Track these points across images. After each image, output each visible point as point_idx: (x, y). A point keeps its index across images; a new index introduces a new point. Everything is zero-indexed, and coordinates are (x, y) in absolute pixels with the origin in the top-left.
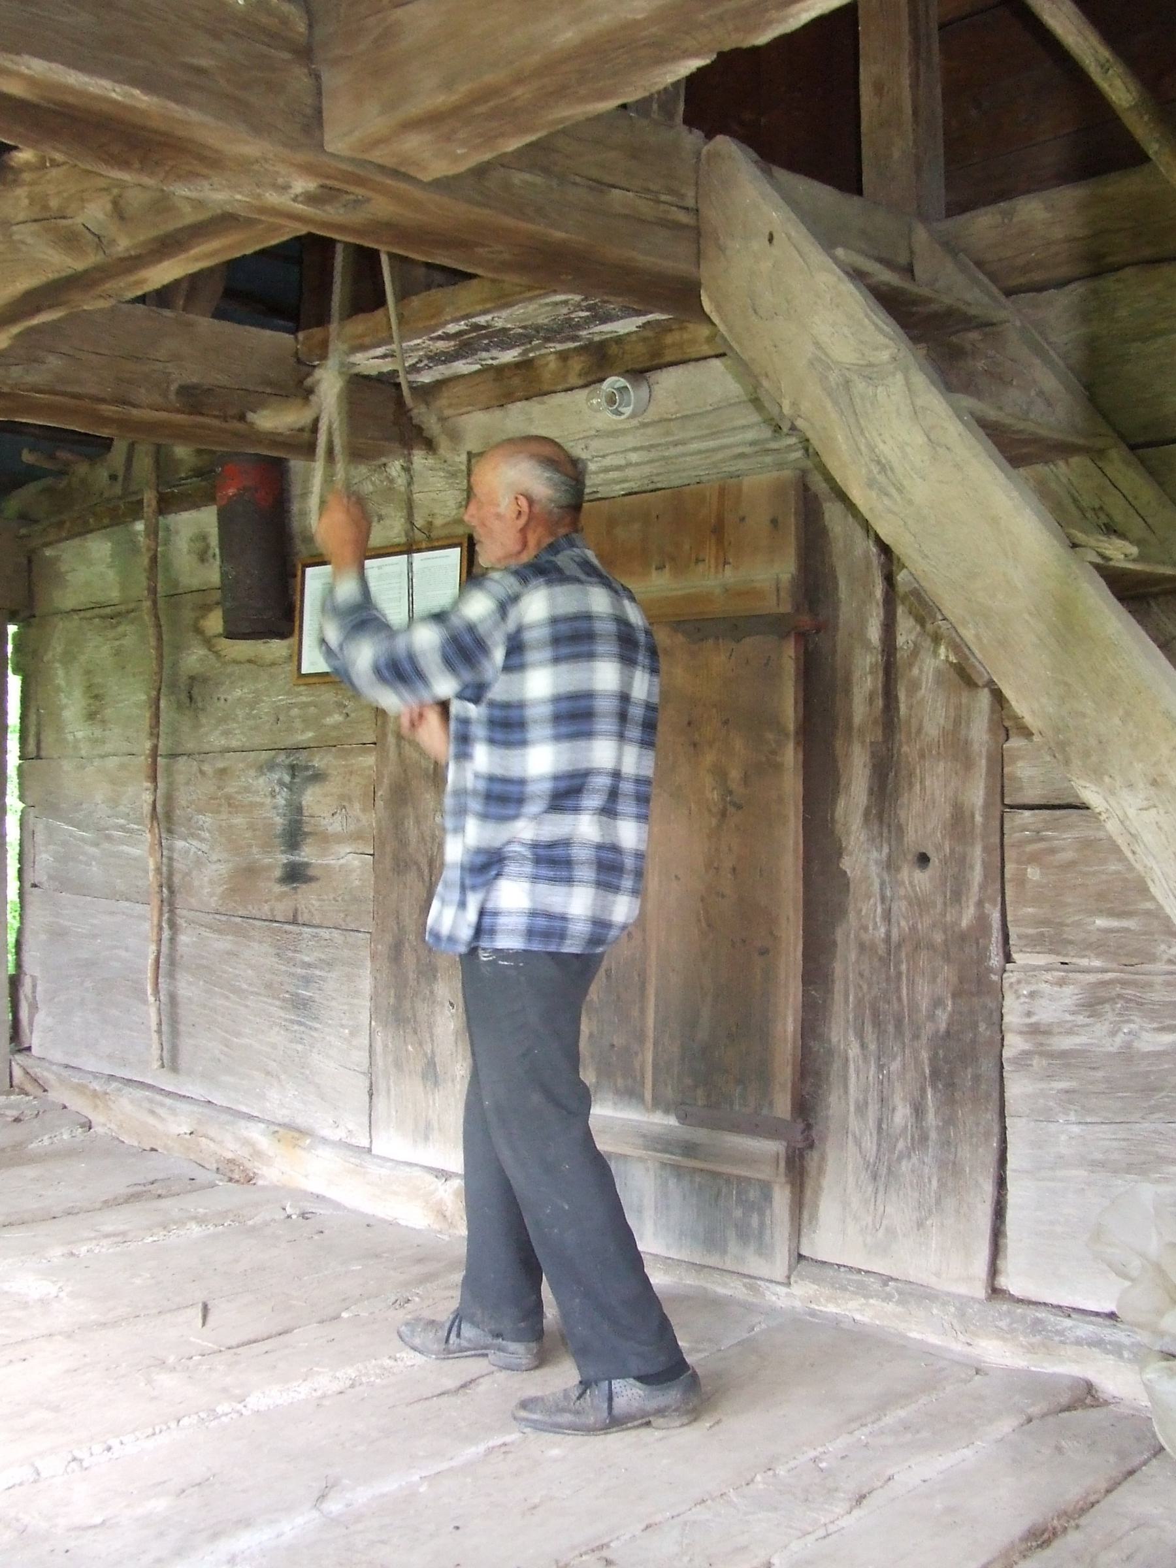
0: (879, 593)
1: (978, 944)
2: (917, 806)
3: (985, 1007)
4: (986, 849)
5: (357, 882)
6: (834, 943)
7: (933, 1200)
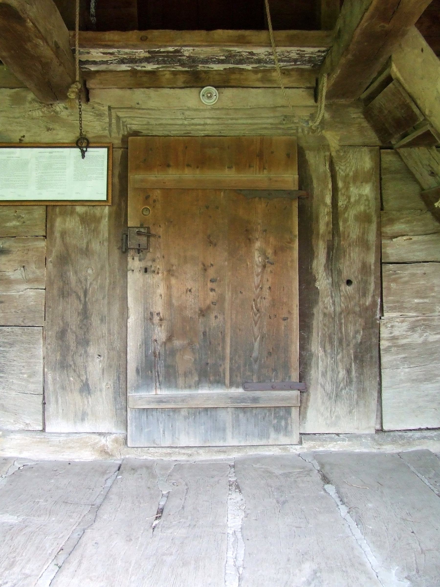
0: (330, 186)
1: (372, 310)
2: (347, 263)
3: (374, 332)
4: (375, 278)
5: (32, 303)
6: (313, 314)
7: (355, 403)
